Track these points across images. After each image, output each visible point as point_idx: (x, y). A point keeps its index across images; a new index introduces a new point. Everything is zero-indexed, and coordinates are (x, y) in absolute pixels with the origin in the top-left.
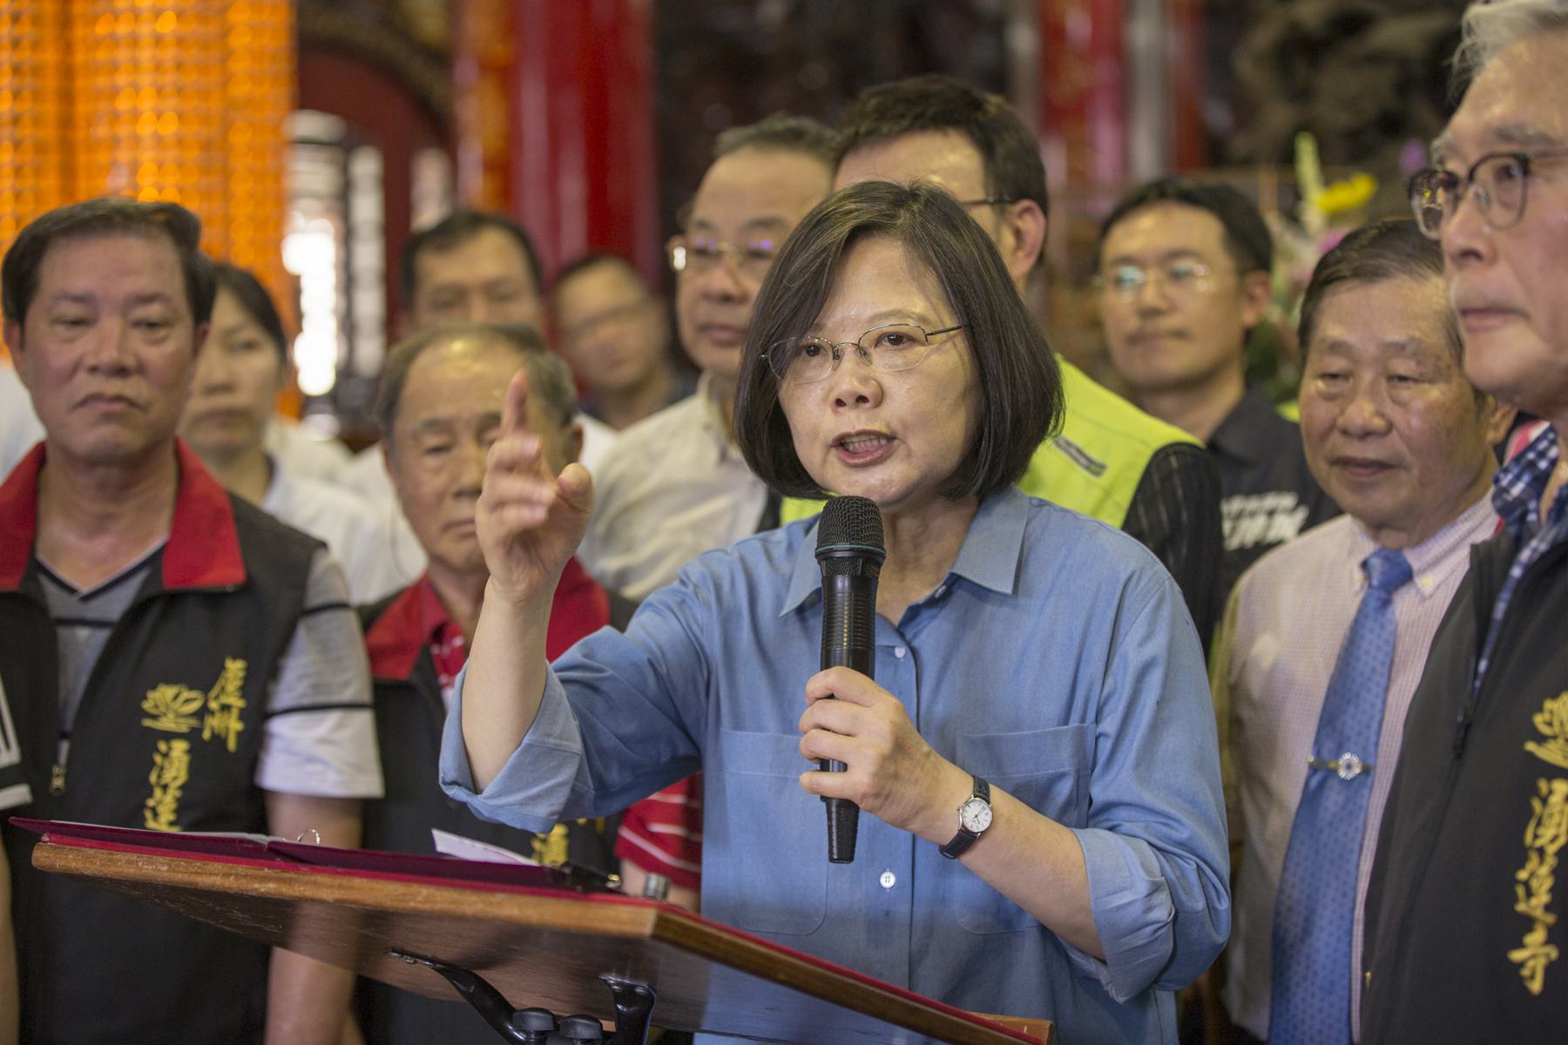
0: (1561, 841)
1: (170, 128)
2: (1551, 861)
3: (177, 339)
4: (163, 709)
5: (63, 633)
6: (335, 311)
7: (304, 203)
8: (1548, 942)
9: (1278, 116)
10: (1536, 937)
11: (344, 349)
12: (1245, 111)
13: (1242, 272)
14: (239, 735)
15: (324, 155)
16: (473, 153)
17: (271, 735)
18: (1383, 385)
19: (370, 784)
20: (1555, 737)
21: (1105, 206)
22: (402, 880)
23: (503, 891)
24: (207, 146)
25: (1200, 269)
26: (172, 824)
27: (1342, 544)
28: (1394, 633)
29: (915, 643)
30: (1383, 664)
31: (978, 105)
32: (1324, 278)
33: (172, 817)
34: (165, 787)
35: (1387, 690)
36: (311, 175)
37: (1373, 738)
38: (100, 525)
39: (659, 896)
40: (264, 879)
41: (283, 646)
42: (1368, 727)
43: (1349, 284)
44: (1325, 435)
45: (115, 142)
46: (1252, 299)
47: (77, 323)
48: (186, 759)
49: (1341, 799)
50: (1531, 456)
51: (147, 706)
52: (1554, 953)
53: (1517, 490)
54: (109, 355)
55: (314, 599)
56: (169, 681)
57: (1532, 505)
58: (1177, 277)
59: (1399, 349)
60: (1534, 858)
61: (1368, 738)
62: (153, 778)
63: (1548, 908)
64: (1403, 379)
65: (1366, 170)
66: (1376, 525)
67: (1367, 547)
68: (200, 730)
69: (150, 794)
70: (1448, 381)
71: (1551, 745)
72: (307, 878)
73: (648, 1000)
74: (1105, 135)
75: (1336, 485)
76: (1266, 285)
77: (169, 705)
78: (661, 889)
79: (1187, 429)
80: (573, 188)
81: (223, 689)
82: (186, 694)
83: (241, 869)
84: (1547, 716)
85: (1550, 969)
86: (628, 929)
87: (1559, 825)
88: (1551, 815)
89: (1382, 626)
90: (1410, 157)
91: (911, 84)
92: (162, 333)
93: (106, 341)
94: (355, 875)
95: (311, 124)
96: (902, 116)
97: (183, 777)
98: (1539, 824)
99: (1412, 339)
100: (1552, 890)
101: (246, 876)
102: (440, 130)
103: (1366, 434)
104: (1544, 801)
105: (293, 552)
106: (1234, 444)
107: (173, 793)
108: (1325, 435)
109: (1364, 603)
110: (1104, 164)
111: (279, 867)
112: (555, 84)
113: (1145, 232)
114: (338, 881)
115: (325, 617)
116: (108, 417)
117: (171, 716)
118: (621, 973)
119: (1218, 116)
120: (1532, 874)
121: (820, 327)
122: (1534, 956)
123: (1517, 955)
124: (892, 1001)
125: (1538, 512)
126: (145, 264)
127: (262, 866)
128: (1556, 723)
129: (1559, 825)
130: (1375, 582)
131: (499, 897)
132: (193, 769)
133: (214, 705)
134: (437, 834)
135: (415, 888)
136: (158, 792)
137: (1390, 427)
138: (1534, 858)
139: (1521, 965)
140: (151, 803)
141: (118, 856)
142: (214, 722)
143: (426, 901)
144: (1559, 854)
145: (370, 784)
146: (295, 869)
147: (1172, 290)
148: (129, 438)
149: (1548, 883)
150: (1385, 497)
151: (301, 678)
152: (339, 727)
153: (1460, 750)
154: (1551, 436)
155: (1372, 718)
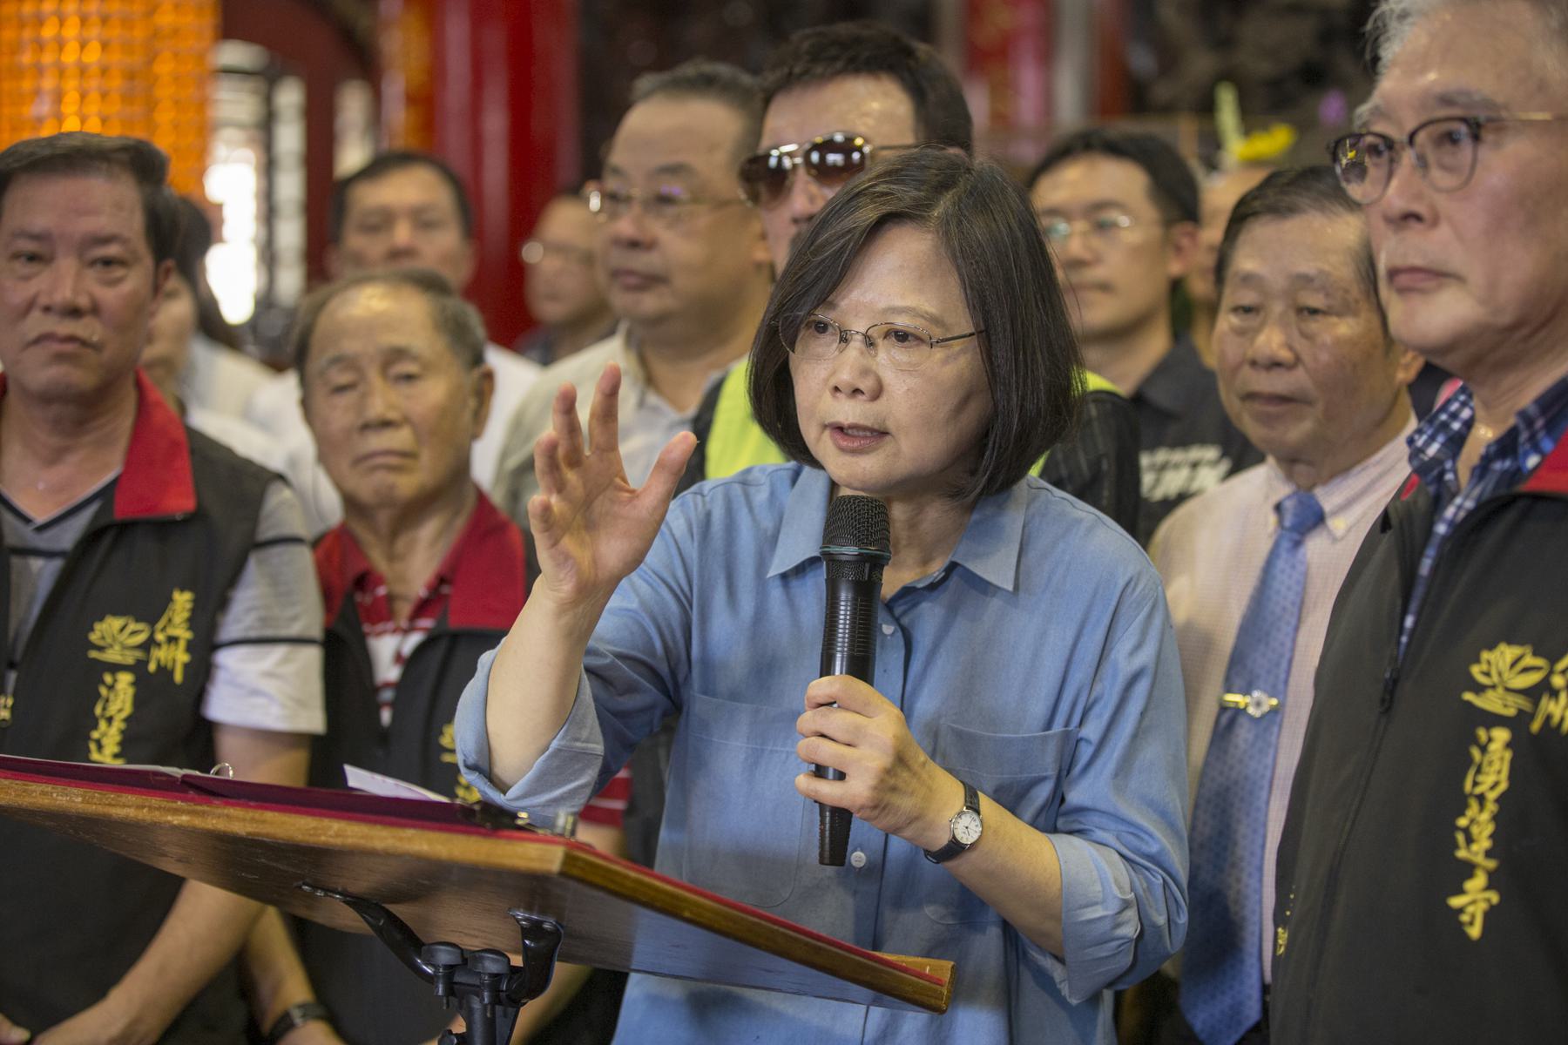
0: (1503, 786)
1: (93, 56)
2: (1491, 807)
3: (134, 281)
4: (109, 640)
5: (16, 561)
6: (255, 241)
7: (228, 134)
8: (1488, 888)
9: (1200, 63)
10: (1477, 883)
11: (264, 280)
12: (1169, 59)
13: (1168, 223)
14: (186, 666)
15: (250, 84)
16: (395, 87)
17: (217, 667)
18: (1292, 316)
19: (313, 721)
20: (1494, 687)
21: (1028, 153)
22: (313, 815)
23: (414, 826)
24: (130, 76)
25: (1124, 221)
26: (116, 756)
27: (1261, 484)
28: (1306, 574)
29: (905, 621)
30: (1293, 604)
31: (909, 53)
32: (1242, 215)
33: (116, 749)
34: (110, 720)
35: (1297, 629)
36: (235, 104)
37: (1282, 676)
38: (55, 457)
39: (567, 834)
40: (177, 811)
41: (234, 578)
42: (1278, 665)
43: (1265, 219)
44: (1236, 369)
45: (39, 70)
46: (1179, 249)
47: (33, 258)
48: (131, 691)
49: (1250, 736)
50: (1444, 417)
51: (94, 637)
52: (1494, 897)
53: (1433, 450)
54: (64, 293)
55: (266, 532)
56: (117, 613)
57: (1448, 465)
58: (1102, 227)
59: (1305, 281)
60: (1474, 804)
61: (1277, 677)
62: (98, 710)
63: (1489, 854)
64: (1314, 312)
65: (1284, 121)
66: (1290, 461)
67: (1283, 490)
68: (147, 663)
69: (95, 726)
70: (1355, 314)
71: (1490, 694)
72: (219, 811)
73: (555, 935)
74: (1028, 78)
75: (1252, 429)
76: (1192, 236)
77: (115, 636)
78: (569, 827)
79: (1112, 381)
80: (496, 123)
81: (170, 620)
82: (133, 626)
83: (155, 801)
84: (1484, 667)
85: (1490, 915)
86: (536, 866)
87: (1499, 772)
88: (1490, 763)
89: (1293, 567)
90: (1330, 107)
91: (844, 29)
92: (118, 272)
93: (65, 280)
94: (267, 808)
95: (235, 54)
96: (835, 59)
97: (128, 710)
98: (1479, 771)
99: (1321, 272)
100: (1492, 836)
101: (159, 808)
102: (363, 61)
103: (1275, 365)
104: (1484, 749)
105: (245, 483)
106: (1161, 396)
107: (118, 725)
108: (1236, 369)
109: (1276, 545)
110: (1026, 108)
111: (192, 800)
112: (479, 16)
113: (1071, 184)
114: (250, 814)
115: (276, 550)
116: (60, 358)
117: (117, 647)
118: (529, 908)
119: (1141, 60)
120: (1472, 821)
121: (833, 306)
122: (1473, 902)
123: (1456, 902)
124: (796, 940)
125: (1455, 472)
126: (111, 204)
127: (178, 798)
128: (1494, 673)
129: (1499, 772)
130: (1287, 523)
131: (410, 832)
132: (138, 701)
133: (160, 637)
134: (349, 769)
135: (326, 822)
136: (103, 725)
137: (1298, 360)
138: (1474, 804)
139: (1461, 910)
140: (95, 735)
141: (34, 787)
142: (161, 655)
143: (337, 835)
144: (1498, 801)
145: (313, 721)
146: (209, 803)
147: (1097, 242)
148: (82, 377)
149: (1490, 828)
150: (1298, 430)
151: (249, 610)
152: (285, 660)
153: (1389, 698)
154: (1462, 398)
155: (1281, 656)
